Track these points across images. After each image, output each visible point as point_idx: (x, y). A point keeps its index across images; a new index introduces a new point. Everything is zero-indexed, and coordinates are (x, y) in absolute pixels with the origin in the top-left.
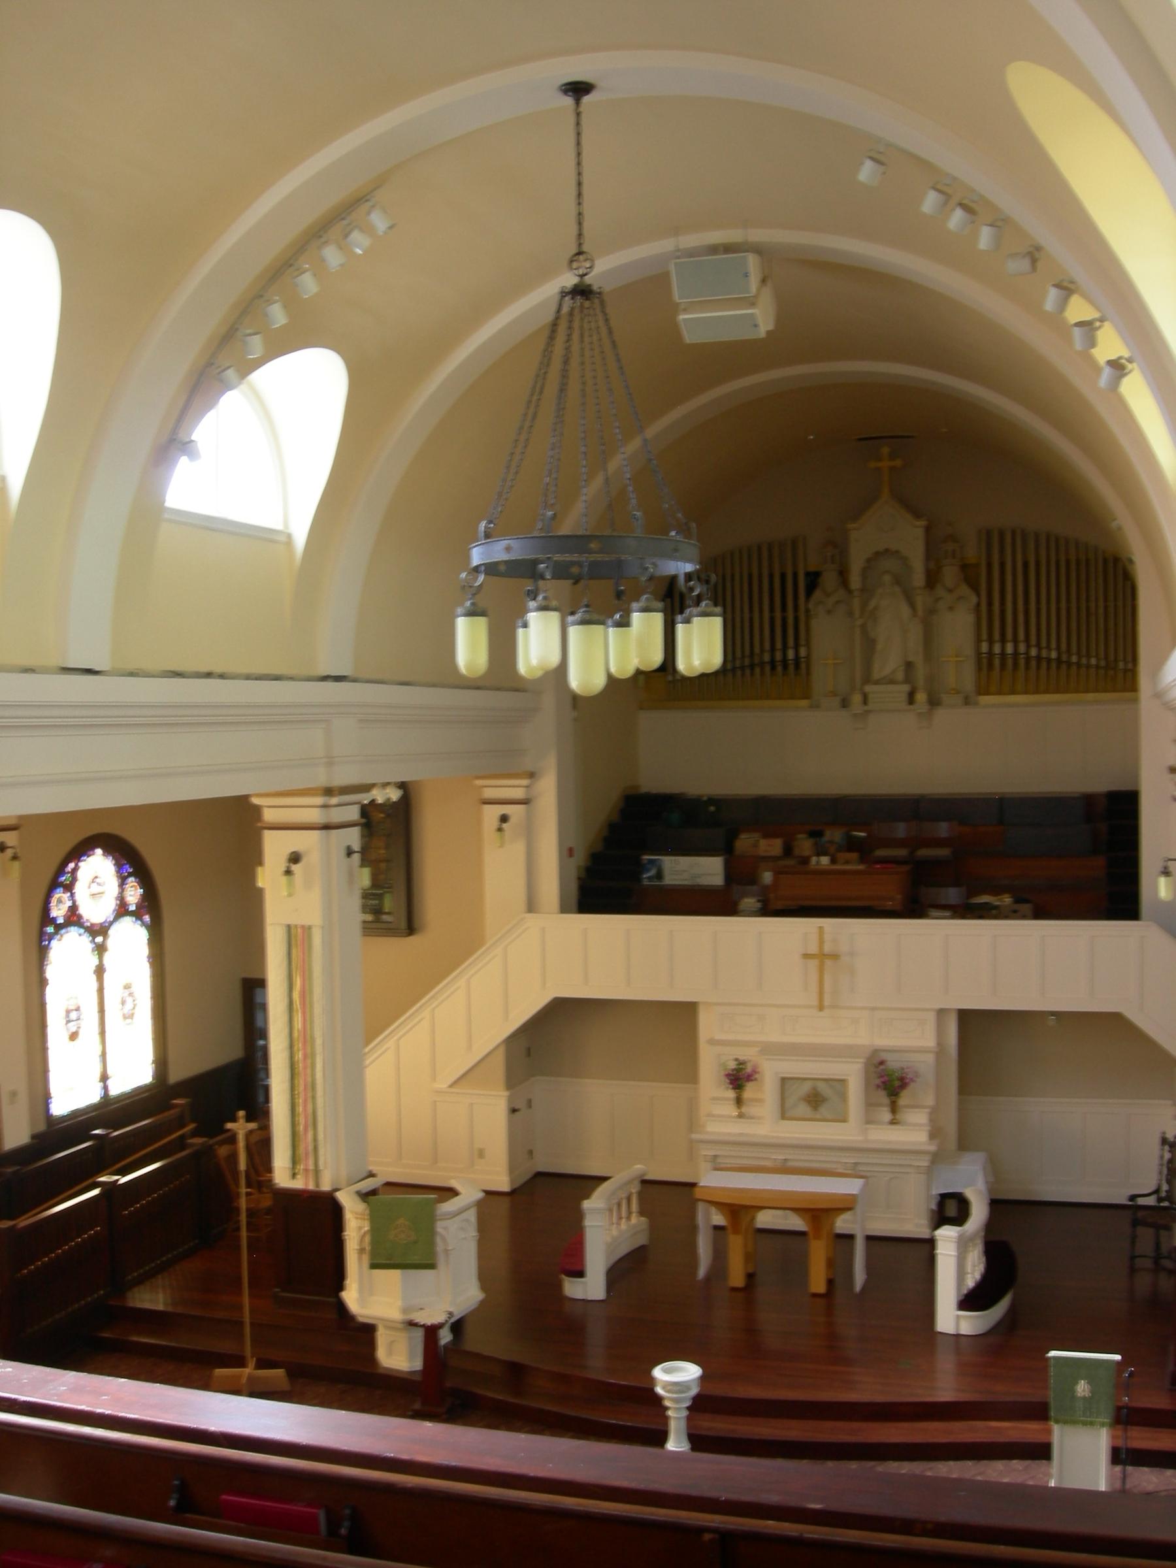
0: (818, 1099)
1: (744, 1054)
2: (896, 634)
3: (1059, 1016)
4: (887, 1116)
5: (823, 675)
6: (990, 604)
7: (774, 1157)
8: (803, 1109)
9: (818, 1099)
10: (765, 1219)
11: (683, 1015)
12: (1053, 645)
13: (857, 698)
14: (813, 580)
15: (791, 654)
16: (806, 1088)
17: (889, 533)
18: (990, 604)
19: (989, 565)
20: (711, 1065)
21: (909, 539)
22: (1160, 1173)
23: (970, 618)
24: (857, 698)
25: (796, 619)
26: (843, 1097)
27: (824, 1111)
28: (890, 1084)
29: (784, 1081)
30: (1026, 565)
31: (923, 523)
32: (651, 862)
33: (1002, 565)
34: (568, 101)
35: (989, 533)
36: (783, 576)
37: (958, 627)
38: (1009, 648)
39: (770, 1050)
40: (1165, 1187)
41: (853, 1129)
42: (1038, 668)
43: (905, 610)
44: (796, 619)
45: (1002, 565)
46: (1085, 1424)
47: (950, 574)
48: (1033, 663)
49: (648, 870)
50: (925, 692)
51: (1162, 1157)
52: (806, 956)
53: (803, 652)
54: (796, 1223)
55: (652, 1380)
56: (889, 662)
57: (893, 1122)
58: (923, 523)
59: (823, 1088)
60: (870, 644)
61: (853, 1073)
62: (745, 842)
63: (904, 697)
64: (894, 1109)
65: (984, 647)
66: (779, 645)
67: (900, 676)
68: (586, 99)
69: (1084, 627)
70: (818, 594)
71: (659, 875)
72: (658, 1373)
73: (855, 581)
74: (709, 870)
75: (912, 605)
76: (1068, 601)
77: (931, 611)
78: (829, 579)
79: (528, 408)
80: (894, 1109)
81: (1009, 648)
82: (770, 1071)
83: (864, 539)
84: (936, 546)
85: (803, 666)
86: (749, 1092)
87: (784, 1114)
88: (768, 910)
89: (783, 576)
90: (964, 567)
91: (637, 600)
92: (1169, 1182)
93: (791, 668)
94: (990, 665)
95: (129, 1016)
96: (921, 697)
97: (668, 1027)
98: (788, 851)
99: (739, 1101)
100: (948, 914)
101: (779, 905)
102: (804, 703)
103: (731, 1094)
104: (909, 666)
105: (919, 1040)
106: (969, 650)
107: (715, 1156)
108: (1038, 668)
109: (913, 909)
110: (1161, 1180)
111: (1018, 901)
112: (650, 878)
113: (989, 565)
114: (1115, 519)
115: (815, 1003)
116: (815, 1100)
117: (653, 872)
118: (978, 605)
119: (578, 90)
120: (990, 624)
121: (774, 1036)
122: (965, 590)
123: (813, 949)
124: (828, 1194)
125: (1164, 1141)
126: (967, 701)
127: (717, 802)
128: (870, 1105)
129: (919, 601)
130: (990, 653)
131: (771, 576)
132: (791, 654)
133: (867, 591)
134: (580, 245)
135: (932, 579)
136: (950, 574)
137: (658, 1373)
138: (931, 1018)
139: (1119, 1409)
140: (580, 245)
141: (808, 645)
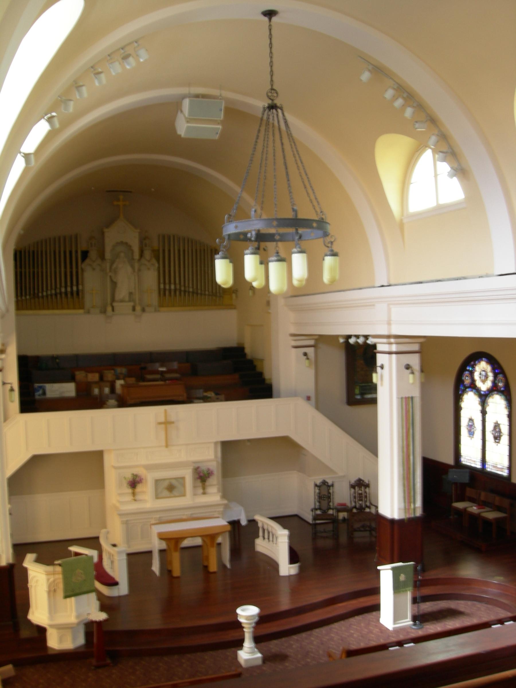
0: (172, 488)
1: (135, 471)
2: (125, 280)
3: (249, 440)
4: (201, 491)
5: (88, 299)
6: (164, 267)
7: (217, 510)
8: (166, 493)
9: (172, 488)
10: (186, 543)
11: (96, 457)
12: (191, 285)
13: (109, 309)
14: (85, 255)
15: (75, 288)
16: (166, 484)
17: (122, 234)
18: (164, 267)
19: (164, 251)
20: (112, 478)
21: (133, 238)
22: (315, 499)
23: (156, 273)
24: (109, 309)
25: (77, 272)
26: (184, 485)
27: (175, 493)
28: (202, 477)
29: (157, 482)
30: (179, 251)
31: (138, 230)
32: (40, 387)
33: (169, 251)
34: (266, 19)
35: (164, 237)
36: (71, 252)
37: (150, 277)
38: (173, 287)
39: (149, 468)
40: (318, 504)
41: (190, 499)
42: (185, 295)
43: (129, 269)
44: (77, 272)
45: (169, 251)
46: (403, 591)
47: (147, 254)
48: (182, 293)
49: (38, 391)
50: (139, 307)
51: (315, 492)
52: (160, 423)
53: (80, 287)
54: (198, 541)
55: (236, 615)
56: (122, 293)
57: (204, 493)
58: (138, 230)
59: (174, 482)
60: (114, 284)
61: (188, 475)
62: (80, 375)
63: (131, 308)
64: (204, 488)
65: (162, 286)
66: (58, 286)
67: (127, 299)
68: (274, 19)
69: (195, 279)
70: (88, 261)
71: (44, 393)
72: (239, 611)
73: (108, 255)
74: (68, 389)
75: (133, 267)
76: (197, 267)
77: (139, 270)
78: (93, 254)
79: (266, 157)
80: (204, 488)
81: (173, 287)
82: (150, 478)
83: (113, 236)
84: (143, 240)
85: (80, 294)
86: (139, 488)
87: (157, 497)
88: (123, 403)
89: (71, 252)
90: (153, 251)
91: (248, 249)
92: (319, 502)
93: (69, 295)
94: (165, 294)
95: (471, 420)
96: (138, 308)
97: (89, 465)
98: (101, 378)
99: (134, 494)
100: (202, 401)
101: (132, 402)
102: (81, 311)
103: (130, 491)
104: (131, 294)
105: (209, 456)
106: (155, 287)
107: (127, 521)
108: (185, 295)
109: (189, 400)
110: (315, 502)
111: (217, 394)
112: (39, 395)
113: (164, 251)
114: (296, 228)
115: (163, 443)
116: (171, 488)
117: (41, 392)
118: (159, 268)
119: (270, 14)
120: (164, 276)
121: (144, 462)
122: (154, 261)
123: (162, 419)
124: (187, 530)
125: (316, 485)
126: (156, 311)
127: (54, 358)
128: (195, 487)
129: (136, 265)
130: (165, 289)
131: (65, 252)
132: (75, 288)
133: (112, 263)
134: (272, 85)
135: (142, 255)
136: (147, 254)
137: (239, 611)
138: (212, 445)
139: (415, 582)
140: (272, 85)
141: (83, 285)
